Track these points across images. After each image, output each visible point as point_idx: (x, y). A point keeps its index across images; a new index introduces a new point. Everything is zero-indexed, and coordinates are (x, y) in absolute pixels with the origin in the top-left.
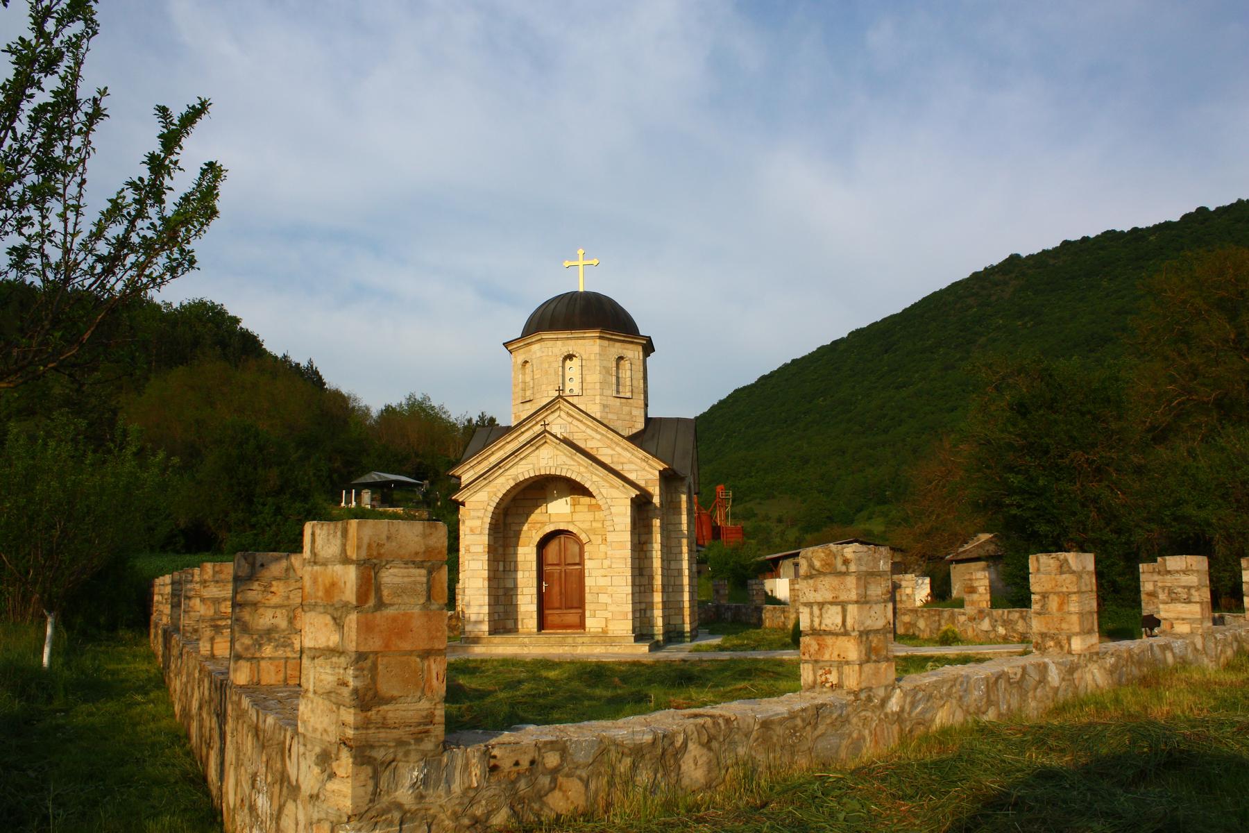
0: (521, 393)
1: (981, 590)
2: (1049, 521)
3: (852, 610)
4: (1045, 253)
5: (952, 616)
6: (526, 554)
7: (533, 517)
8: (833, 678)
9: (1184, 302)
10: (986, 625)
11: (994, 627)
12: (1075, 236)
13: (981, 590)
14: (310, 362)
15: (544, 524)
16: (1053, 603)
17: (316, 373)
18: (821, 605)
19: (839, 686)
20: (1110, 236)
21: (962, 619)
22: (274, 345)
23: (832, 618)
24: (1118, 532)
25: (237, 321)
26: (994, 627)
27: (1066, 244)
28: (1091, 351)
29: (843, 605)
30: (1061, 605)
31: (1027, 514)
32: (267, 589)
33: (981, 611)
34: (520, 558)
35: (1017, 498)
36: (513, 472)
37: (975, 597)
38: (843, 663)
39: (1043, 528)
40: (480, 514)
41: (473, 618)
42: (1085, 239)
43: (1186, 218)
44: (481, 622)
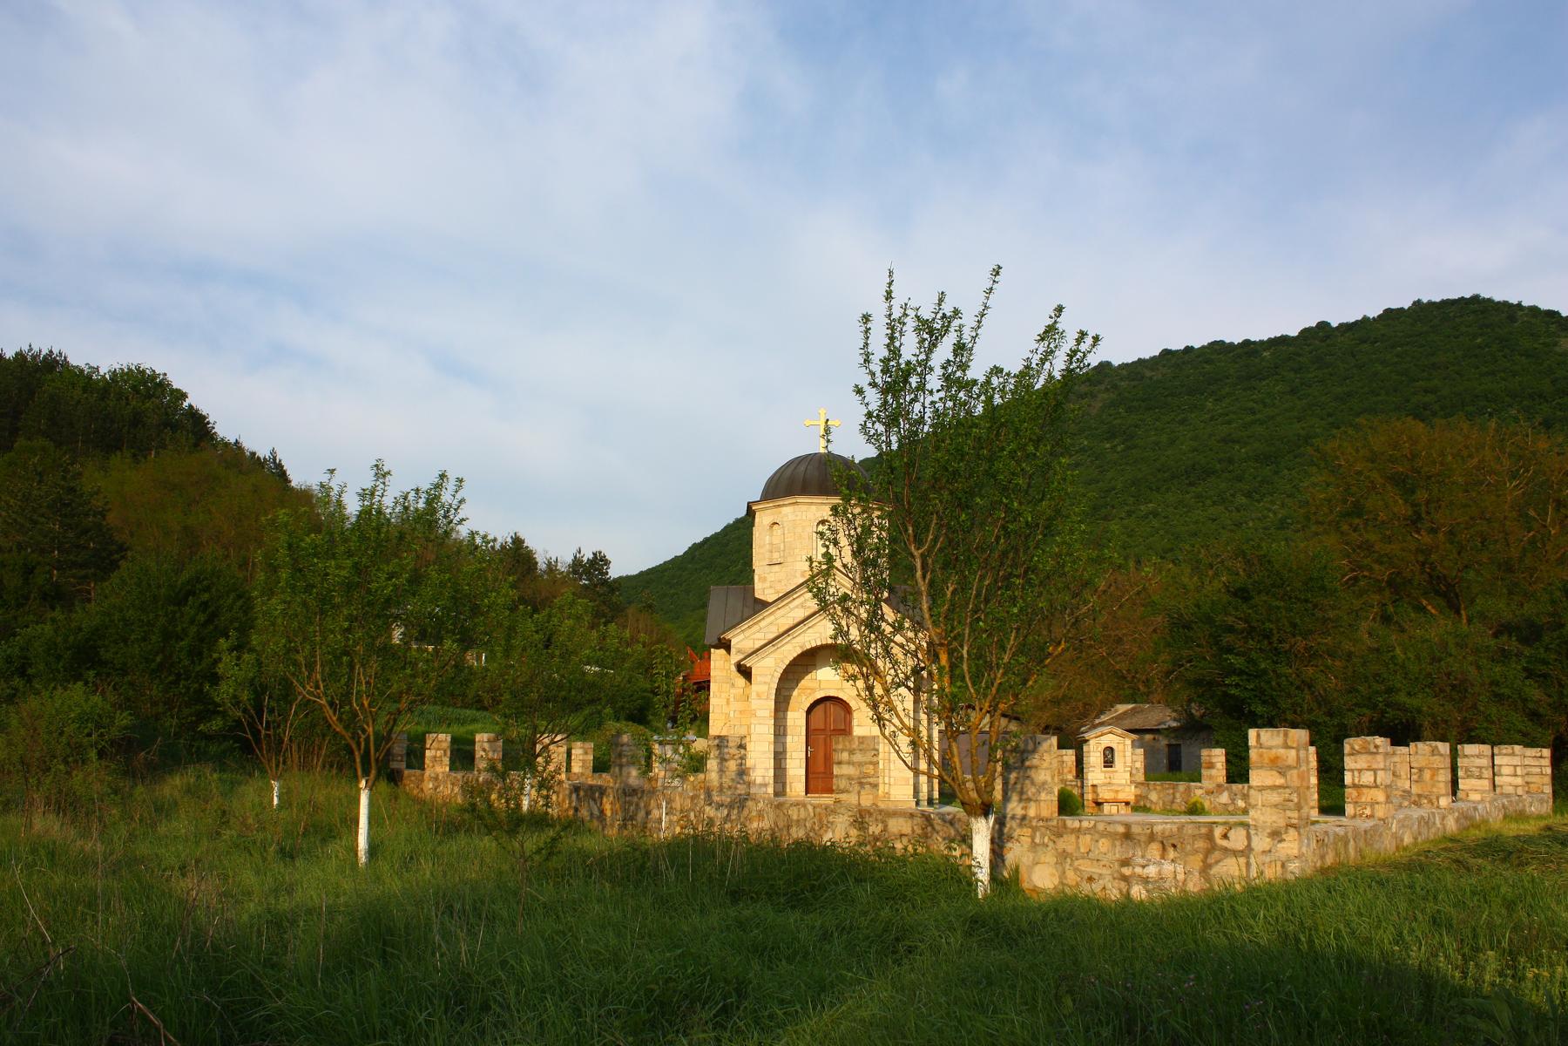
0: (767, 555)
1: (1219, 766)
2: (1264, 702)
3: (1380, 774)
4: (1140, 361)
5: (1188, 790)
6: (796, 719)
7: (803, 683)
8: (1368, 811)
9: (1359, 473)
10: (1224, 798)
11: (1233, 801)
12: (1177, 345)
13: (1219, 766)
14: (273, 452)
15: (813, 690)
16: (1427, 775)
17: (279, 466)
18: (1360, 771)
19: (1371, 816)
20: (1218, 347)
21: (1199, 792)
22: (225, 429)
23: (1367, 778)
24: (1330, 714)
25: (184, 396)
26: (1233, 801)
27: (1166, 353)
28: (1191, 484)
29: (1375, 771)
30: (1433, 776)
31: (1246, 695)
32: (1042, 759)
33: (1219, 786)
34: (789, 722)
35: (1235, 679)
36: (800, 640)
37: (1214, 772)
38: (1373, 804)
39: (1260, 709)
40: (768, 679)
41: (759, 780)
42: (1189, 349)
43: (1306, 332)
44: (766, 785)
